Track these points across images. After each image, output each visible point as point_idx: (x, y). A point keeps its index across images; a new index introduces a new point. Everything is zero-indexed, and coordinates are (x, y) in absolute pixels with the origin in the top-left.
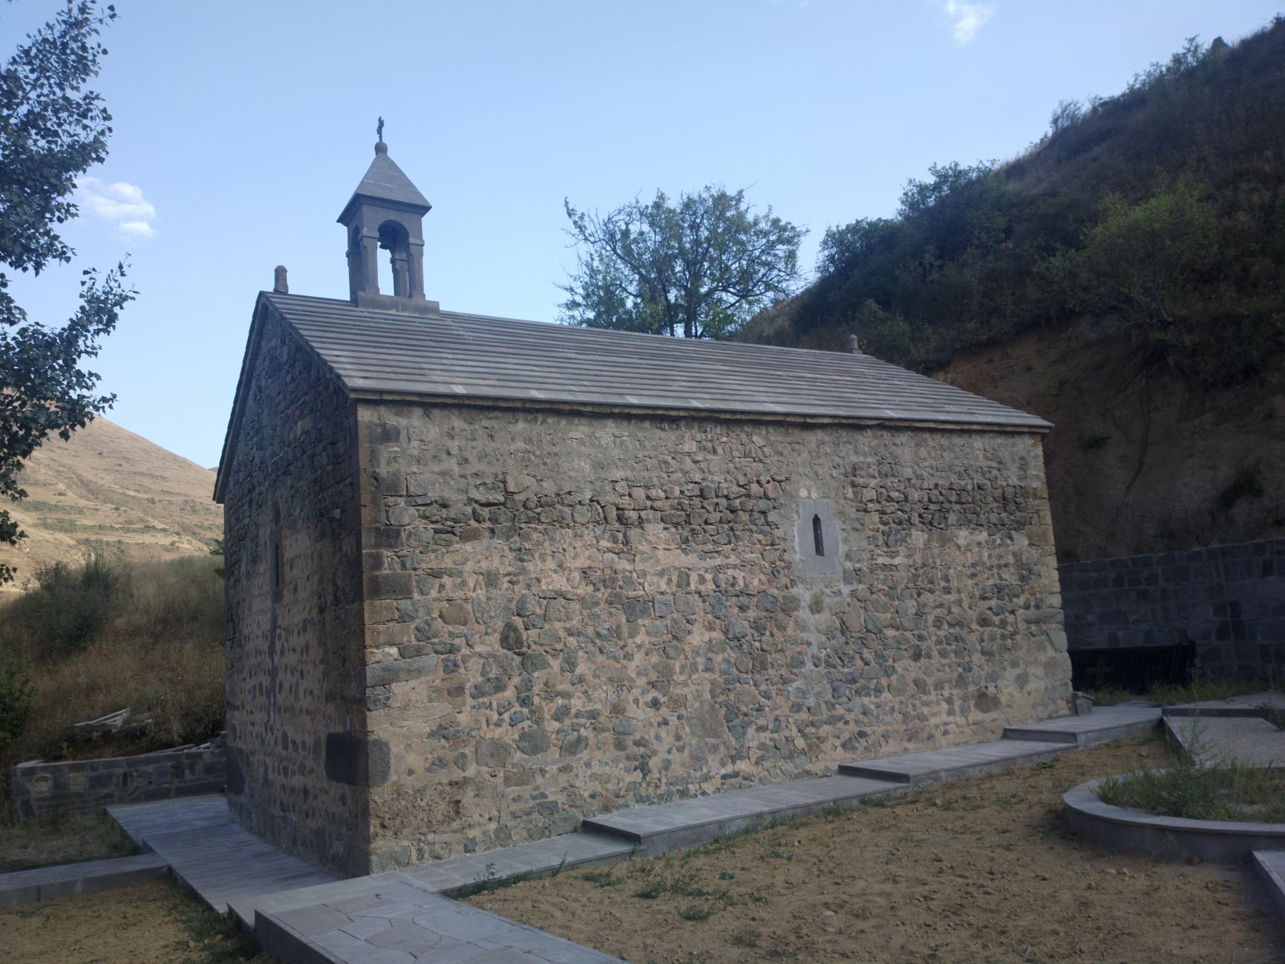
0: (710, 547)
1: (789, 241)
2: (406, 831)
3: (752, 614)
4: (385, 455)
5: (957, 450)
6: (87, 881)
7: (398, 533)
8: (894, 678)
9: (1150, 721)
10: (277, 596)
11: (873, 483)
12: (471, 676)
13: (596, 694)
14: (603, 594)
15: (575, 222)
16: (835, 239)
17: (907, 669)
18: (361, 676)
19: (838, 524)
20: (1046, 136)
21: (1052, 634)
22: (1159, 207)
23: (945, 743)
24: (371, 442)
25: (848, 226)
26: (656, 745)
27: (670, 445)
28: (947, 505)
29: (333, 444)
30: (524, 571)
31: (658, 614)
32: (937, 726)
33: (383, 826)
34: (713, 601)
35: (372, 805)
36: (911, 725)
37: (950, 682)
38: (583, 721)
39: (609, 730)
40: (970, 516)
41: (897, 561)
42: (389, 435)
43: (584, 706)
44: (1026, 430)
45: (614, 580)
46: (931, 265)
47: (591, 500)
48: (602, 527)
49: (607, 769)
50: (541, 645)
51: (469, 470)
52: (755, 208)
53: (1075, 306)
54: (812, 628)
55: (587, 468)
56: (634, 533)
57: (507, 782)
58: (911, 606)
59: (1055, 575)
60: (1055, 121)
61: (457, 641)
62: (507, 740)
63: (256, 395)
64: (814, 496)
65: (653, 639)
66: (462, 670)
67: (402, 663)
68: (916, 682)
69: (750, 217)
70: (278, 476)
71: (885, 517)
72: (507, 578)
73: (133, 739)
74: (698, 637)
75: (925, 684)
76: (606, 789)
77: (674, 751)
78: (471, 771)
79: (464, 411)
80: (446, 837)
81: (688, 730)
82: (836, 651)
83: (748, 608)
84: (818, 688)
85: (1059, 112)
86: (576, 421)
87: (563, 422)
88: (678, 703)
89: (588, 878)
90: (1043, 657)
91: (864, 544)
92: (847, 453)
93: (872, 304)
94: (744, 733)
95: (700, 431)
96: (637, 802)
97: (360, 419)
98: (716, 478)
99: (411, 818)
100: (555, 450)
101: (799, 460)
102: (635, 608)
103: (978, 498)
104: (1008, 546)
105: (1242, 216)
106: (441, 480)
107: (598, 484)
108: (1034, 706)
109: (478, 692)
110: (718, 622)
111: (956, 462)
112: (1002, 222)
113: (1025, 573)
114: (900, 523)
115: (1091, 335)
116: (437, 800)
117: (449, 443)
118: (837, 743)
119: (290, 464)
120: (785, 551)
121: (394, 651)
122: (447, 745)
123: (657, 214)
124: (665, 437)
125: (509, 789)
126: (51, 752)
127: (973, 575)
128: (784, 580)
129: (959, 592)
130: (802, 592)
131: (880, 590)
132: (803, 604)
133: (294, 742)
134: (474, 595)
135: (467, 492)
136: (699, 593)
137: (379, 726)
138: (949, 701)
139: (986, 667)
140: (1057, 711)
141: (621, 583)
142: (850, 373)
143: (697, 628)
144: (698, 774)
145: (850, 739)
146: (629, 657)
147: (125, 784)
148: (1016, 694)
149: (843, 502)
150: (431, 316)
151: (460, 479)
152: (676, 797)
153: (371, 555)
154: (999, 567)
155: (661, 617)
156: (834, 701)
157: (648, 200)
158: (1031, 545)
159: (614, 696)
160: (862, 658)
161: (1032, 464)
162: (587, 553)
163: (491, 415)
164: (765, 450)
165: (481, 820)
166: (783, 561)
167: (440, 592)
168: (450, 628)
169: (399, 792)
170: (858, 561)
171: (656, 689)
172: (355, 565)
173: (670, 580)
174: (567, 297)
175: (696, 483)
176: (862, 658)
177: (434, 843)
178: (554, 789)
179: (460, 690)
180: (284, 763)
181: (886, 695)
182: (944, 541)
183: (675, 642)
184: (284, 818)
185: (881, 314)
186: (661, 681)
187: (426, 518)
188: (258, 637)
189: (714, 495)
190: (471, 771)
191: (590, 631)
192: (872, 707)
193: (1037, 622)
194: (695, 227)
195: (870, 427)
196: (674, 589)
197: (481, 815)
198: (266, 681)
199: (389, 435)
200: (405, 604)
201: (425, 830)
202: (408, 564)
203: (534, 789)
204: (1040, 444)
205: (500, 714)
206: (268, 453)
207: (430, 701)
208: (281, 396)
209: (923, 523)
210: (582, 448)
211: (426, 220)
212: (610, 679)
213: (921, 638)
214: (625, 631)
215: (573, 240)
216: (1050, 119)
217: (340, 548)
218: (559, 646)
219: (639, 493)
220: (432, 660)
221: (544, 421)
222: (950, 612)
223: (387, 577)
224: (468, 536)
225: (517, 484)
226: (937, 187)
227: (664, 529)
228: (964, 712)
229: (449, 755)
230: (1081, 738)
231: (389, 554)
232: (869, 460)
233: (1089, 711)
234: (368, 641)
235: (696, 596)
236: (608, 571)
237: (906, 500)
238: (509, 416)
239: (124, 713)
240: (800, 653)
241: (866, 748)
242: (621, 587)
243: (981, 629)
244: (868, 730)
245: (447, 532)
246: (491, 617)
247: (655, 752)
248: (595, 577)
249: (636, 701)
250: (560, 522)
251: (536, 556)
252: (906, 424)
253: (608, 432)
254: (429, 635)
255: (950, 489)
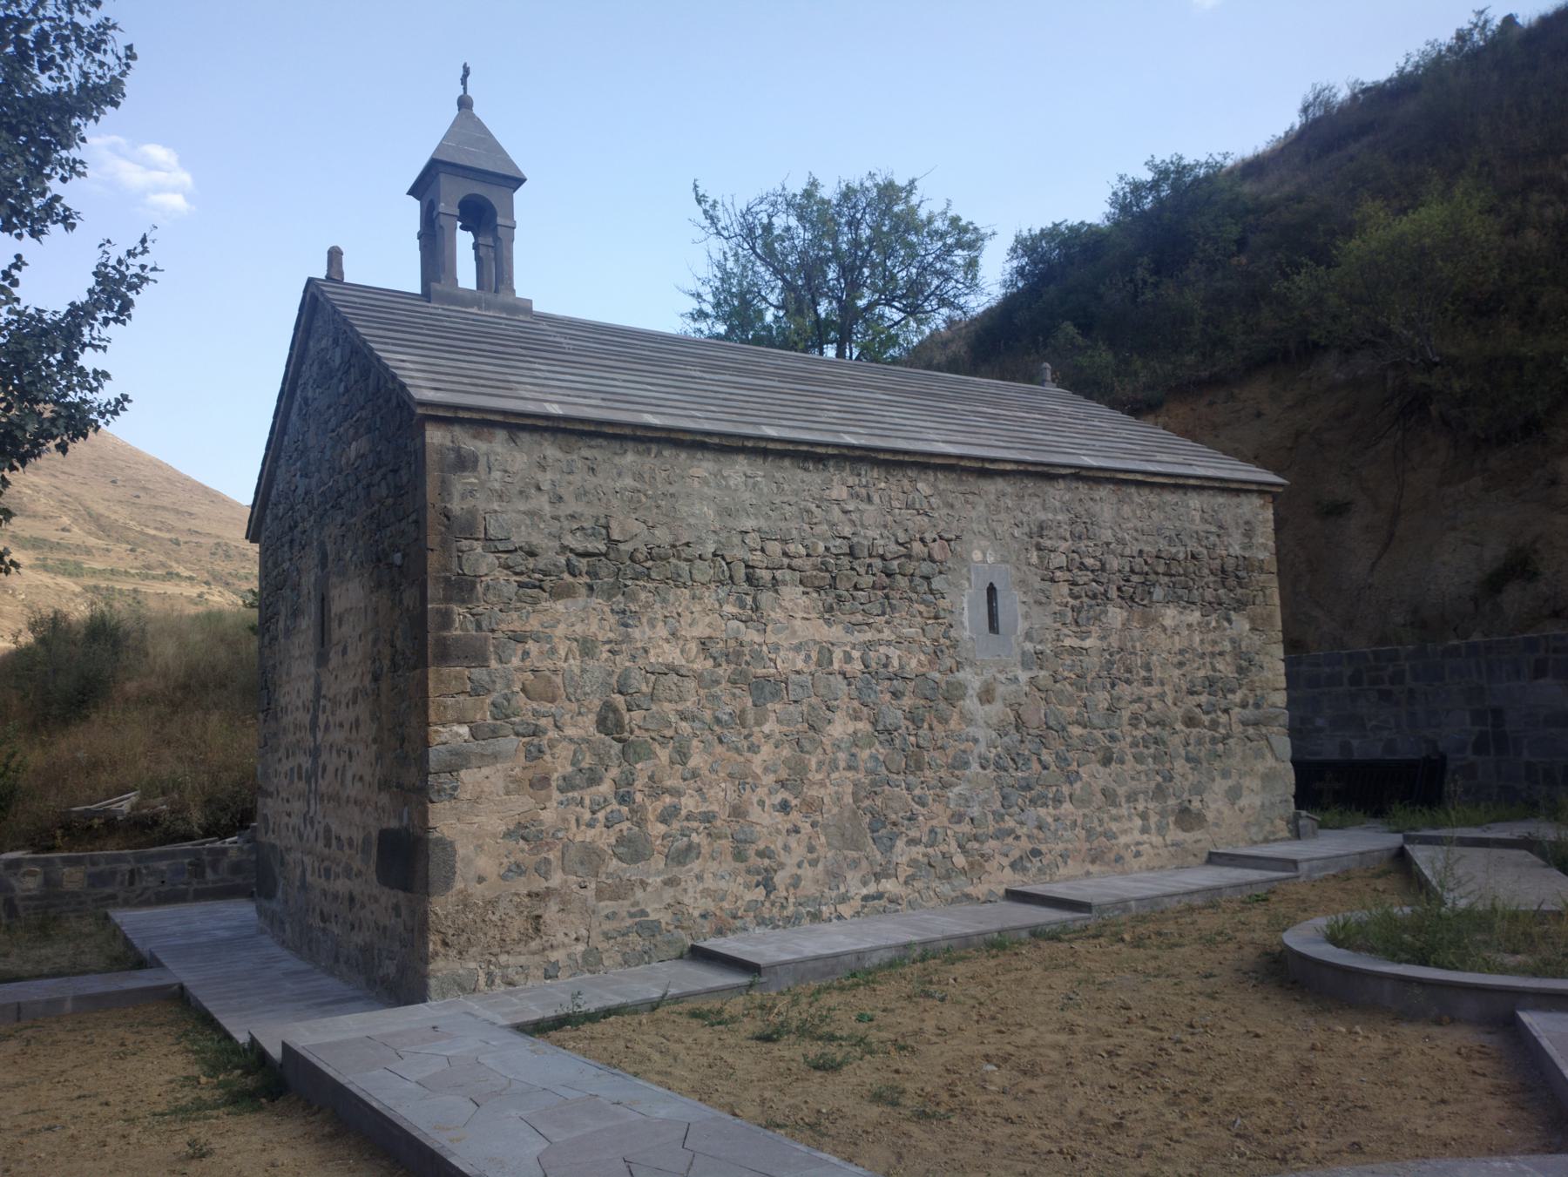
0: (859, 617)
1: (970, 246)
2: (472, 950)
3: (907, 702)
4: (459, 487)
5: (1168, 509)
6: (78, 999)
7: (473, 586)
8: (1078, 785)
9: (1389, 850)
10: (322, 659)
11: (1063, 546)
12: (559, 764)
13: (712, 792)
14: (725, 670)
15: (705, 212)
16: (1027, 247)
17: (1094, 775)
18: (423, 759)
19: (1018, 595)
20: (1292, 129)
21: (1273, 739)
22: (1430, 216)
23: (1136, 867)
24: (442, 471)
25: (1042, 230)
26: (783, 857)
27: (815, 491)
28: (1152, 577)
29: (395, 471)
30: (628, 638)
31: (792, 698)
32: (1127, 846)
33: (445, 944)
34: (860, 684)
35: (432, 918)
36: (1095, 844)
37: (1145, 793)
38: (695, 824)
39: (726, 837)
40: (1180, 592)
41: (1087, 643)
42: (464, 462)
43: (697, 807)
44: (1254, 487)
45: (739, 654)
46: (1145, 282)
47: (715, 555)
48: (726, 589)
49: (723, 884)
50: (647, 730)
51: (564, 510)
52: (930, 202)
53: (1320, 337)
54: (981, 722)
55: (710, 513)
56: (766, 597)
57: (600, 895)
58: (1102, 698)
59: (1281, 667)
60: (1305, 110)
61: (543, 722)
62: (601, 844)
63: (300, 409)
64: (990, 559)
65: (785, 729)
66: (548, 757)
67: (474, 746)
68: (1104, 792)
69: (923, 214)
70: (326, 510)
71: (1076, 589)
72: (607, 647)
73: (143, 828)
74: (840, 728)
75: (1115, 794)
76: (721, 908)
77: (806, 864)
78: (556, 879)
79: (560, 436)
80: (522, 960)
81: (823, 839)
82: (1007, 750)
83: (903, 694)
84: (984, 795)
85: (1311, 98)
86: (699, 455)
87: (683, 455)
88: (811, 806)
89: (694, 1014)
90: (1260, 767)
91: (1049, 621)
92: (1033, 509)
93: (1069, 328)
94: (892, 847)
95: (852, 474)
96: (758, 924)
97: (428, 440)
98: (870, 533)
99: (480, 935)
100: (672, 490)
101: (974, 514)
102: (765, 689)
103: (1191, 570)
104: (1225, 629)
105: (1531, 235)
106: (528, 522)
107: (724, 534)
108: (1247, 826)
109: (567, 784)
110: (865, 710)
111: (1167, 524)
112: (1234, 231)
113: (1244, 664)
114: (1094, 597)
115: (1337, 375)
116: (513, 913)
117: (540, 476)
118: (1005, 862)
119: (341, 495)
120: (951, 626)
121: (464, 730)
122: (526, 847)
123: (807, 205)
124: (812, 479)
125: (602, 904)
126: (41, 841)
127: (1181, 664)
128: (949, 662)
129: (1162, 684)
130: (969, 677)
131: (1065, 679)
132: (971, 692)
133: (338, 838)
134: (565, 665)
135: (560, 538)
136: (844, 674)
137: (444, 821)
138: (1144, 816)
139: (1191, 777)
140: (1274, 833)
141: (748, 658)
142: (1040, 410)
143: (839, 717)
144: (834, 894)
145: (1021, 857)
146: (754, 749)
147: (131, 883)
148: (1226, 811)
149: (1025, 568)
150: (521, 317)
151: (552, 522)
152: (806, 921)
153: (438, 611)
154: (1213, 655)
155: (795, 702)
156: (1003, 811)
157: (797, 187)
158: (1253, 629)
159: (735, 795)
160: (1040, 761)
161: (1260, 530)
162: (707, 619)
163: (593, 443)
164: (932, 500)
165: (566, 940)
166: (948, 638)
167: (523, 660)
168: (535, 705)
169: (466, 903)
170: (1040, 642)
171: (786, 789)
172: (418, 622)
173: (808, 657)
174: (693, 305)
175: (844, 538)
176: (1040, 761)
177: (507, 966)
178: (657, 906)
179: (544, 781)
180: (326, 863)
181: (1067, 807)
182: (1147, 621)
183: (811, 733)
184: (324, 930)
185: (1080, 340)
186: (793, 780)
187: (508, 567)
188: (297, 709)
189: (866, 553)
190: (556, 879)
191: (707, 715)
192: (1050, 820)
193: (1256, 724)
194: (854, 224)
195: (1063, 477)
196: (813, 668)
197: (566, 934)
198: (307, 763)
199: (464, 462)
200: (477, 673)
201: (496, 950)
202: (485, 625)
203: (632, 905)
204: (1271, 506)
205: (594, 812)
206: (314, 481)
207: (508, 793)
208: (332, 410)
209: (1123, 598)
210: (706, 489)
211: (519, 196)
212: (730, 775)
213: (1113, 738)
214: (750, 718)
215: (703, 234)
216: (1300, 106)
217: (401, 601)
218: (669, 733)
219: (774, 548)
220: (510, 743)
221: (659, 454)
222: (1150, 708)
223: (458, 639)
224: (559, 593)
225: (623, 530)
226: (1155, 185)
227: (804, 593)
228: (1161, 830)
229: (529, 860)
230: (1304, 867)
231: (461, 611)
232: (1060, 517)
233: (1315, 835)
234: (432, 718)
235: (840, 678)
236: (732, 643)
237: (1103, 569)
238: (616, 445)
239: (133, 797)
240: (964, 752)
241: (1039, 870)
242: (748, 663)
243: (1187, 731)
244: (1043, 848)
245: (535, 587)
246: (586, 694)
247: (782, 866)
248: (717, 648)
249: (761, 803)
250: (675, 580)
251: (644, 620)
252: (1107, 475)
253: (738, 469)
254: (509, 712)
255: (1158, 557)
